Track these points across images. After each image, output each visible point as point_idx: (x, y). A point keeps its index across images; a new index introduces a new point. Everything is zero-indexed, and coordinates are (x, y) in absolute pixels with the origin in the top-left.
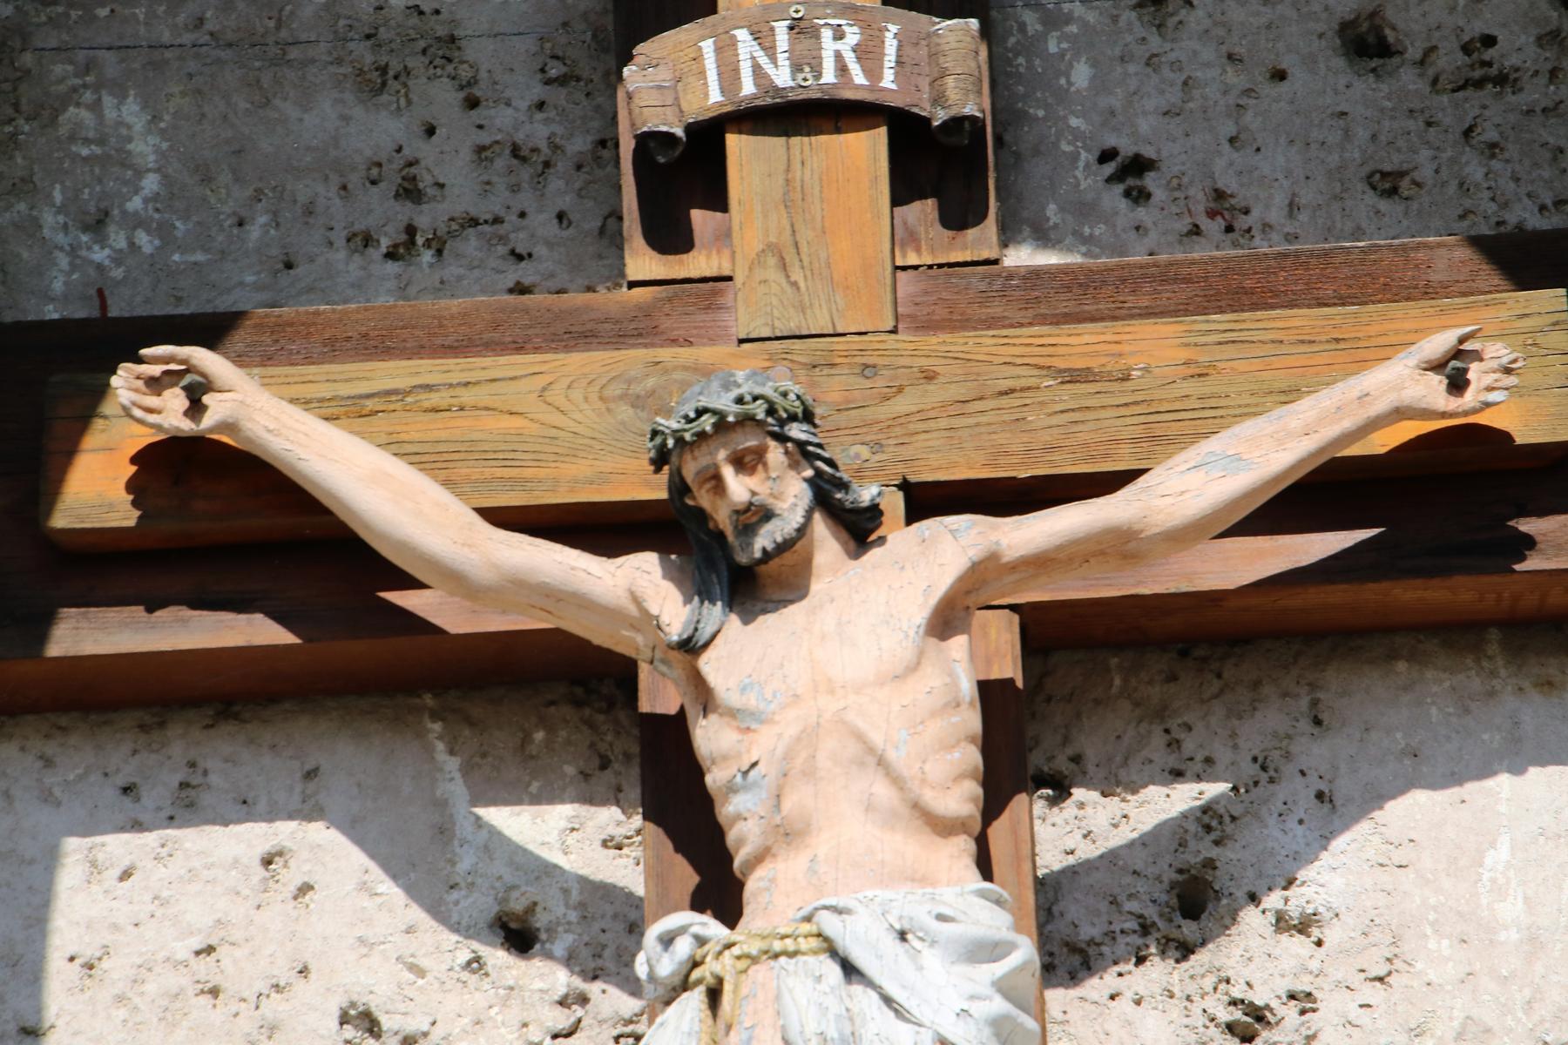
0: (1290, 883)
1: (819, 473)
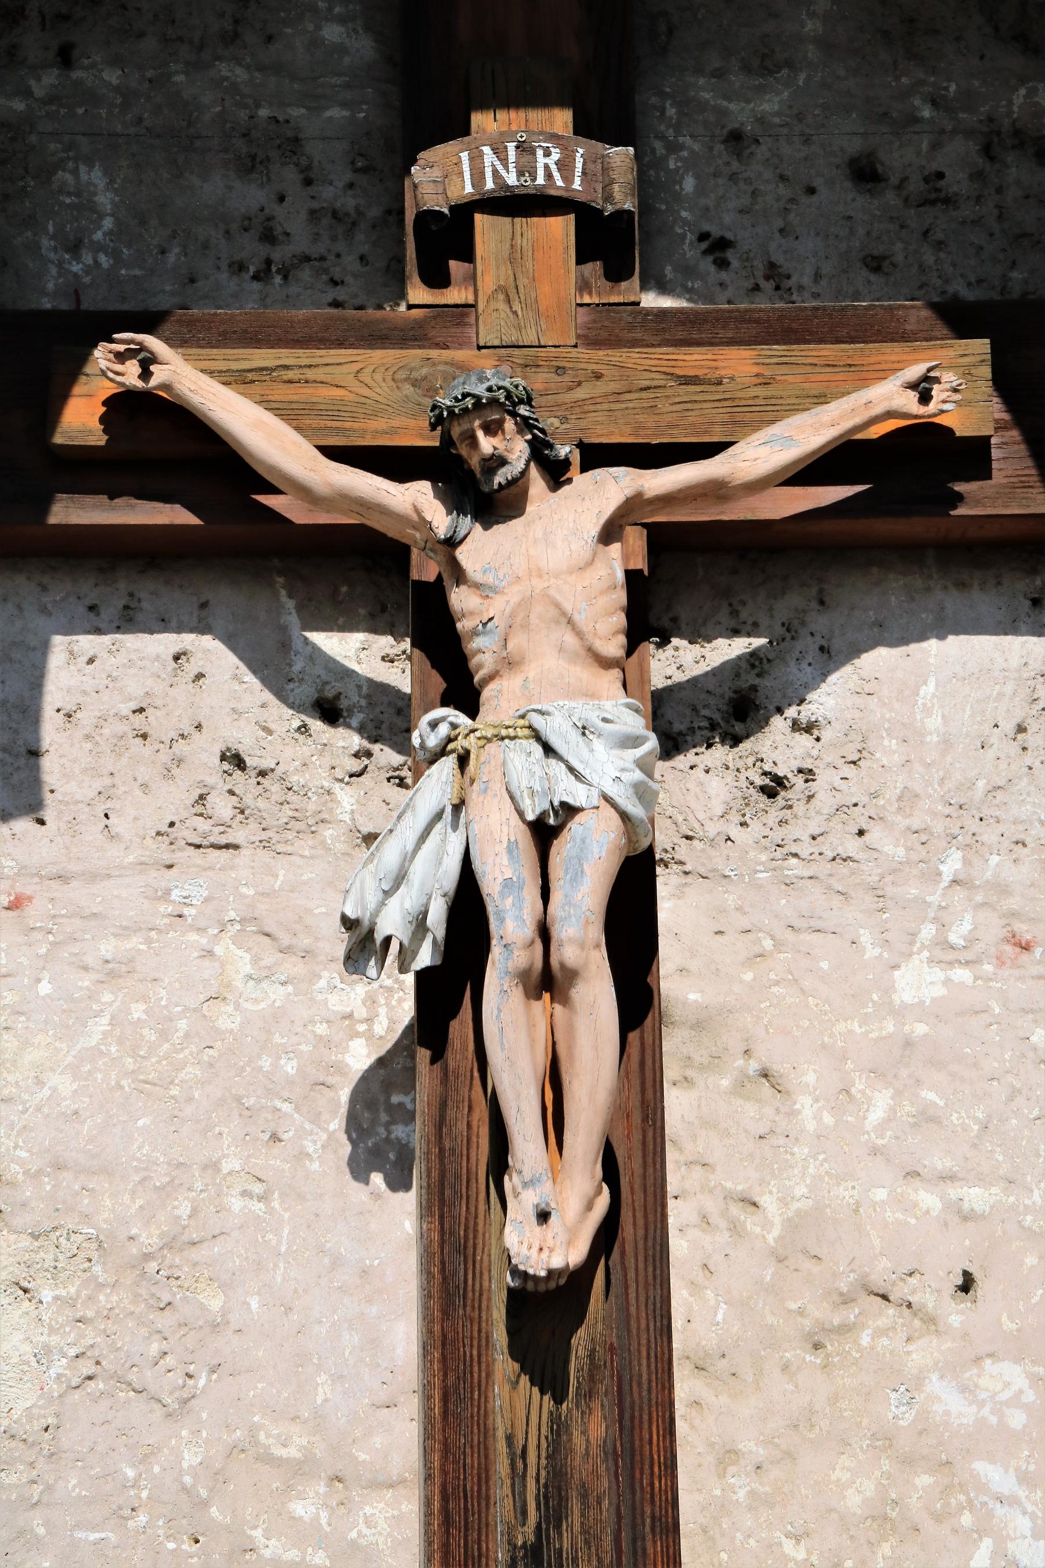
0: (802, 701)
1: (535, 436)
